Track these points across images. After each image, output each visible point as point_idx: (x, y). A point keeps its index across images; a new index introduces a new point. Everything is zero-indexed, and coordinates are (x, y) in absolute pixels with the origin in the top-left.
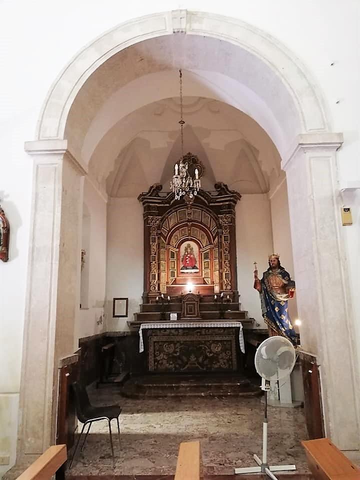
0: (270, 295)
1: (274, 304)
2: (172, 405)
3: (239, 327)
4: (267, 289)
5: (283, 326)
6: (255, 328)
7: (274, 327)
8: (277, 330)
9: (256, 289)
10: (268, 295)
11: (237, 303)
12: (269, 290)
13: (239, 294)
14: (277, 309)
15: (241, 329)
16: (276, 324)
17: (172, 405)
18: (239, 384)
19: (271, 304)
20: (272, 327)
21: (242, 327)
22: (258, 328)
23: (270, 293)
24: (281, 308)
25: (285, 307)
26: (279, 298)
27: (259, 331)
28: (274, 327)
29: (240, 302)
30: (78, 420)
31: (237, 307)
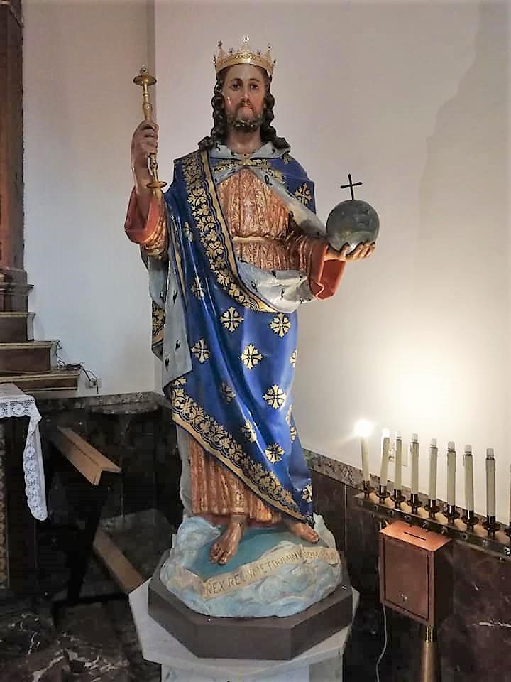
0: (222, 279)
1: (240, 329)
2: (315, 598)
3: (26, 419)
4: (199, 249)
5: (269, 439)
6: (82, 392)
7: (225, 444)
8: (239, 464)
9: (132, 238)
10: (208, 276)
11: (21, 314)
12: (214, 249)
13: (30, 282)
14: (248, 356)
15: (33, 427)
16: (240, 437)
17: (315, 598)
18: (477, 589)
19: (220, 326)
20: (215, 445)
21: (35, 416)
22: (92, 392)
23: (227, 267)
24: (271, 346)
25: (289, 342)
26: (266, 296)
27: (92, 402)
28: (225, 444)
29: (30, 310)
30: (353, 588)
31: (20, 330)
